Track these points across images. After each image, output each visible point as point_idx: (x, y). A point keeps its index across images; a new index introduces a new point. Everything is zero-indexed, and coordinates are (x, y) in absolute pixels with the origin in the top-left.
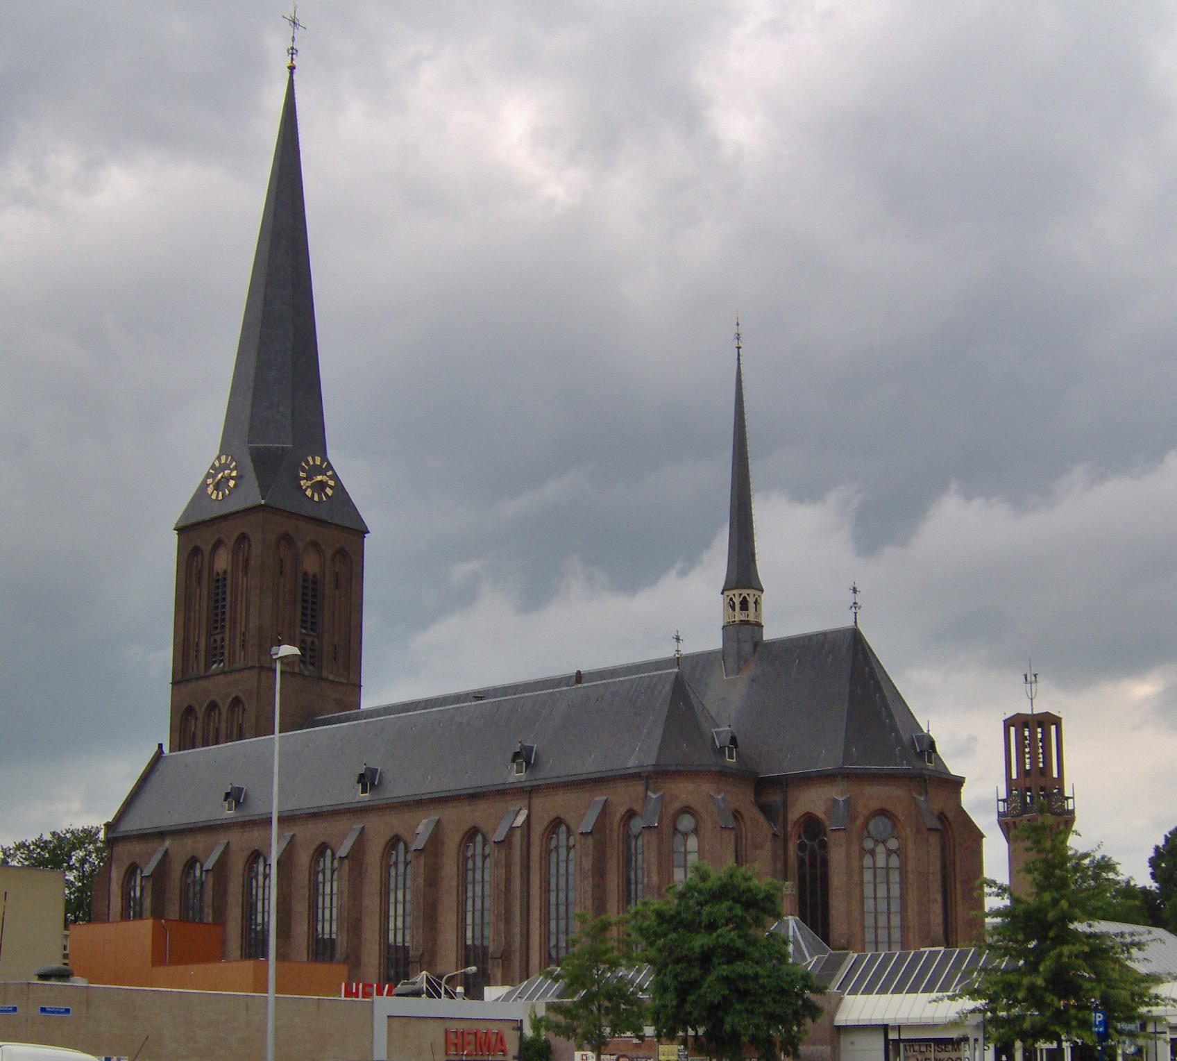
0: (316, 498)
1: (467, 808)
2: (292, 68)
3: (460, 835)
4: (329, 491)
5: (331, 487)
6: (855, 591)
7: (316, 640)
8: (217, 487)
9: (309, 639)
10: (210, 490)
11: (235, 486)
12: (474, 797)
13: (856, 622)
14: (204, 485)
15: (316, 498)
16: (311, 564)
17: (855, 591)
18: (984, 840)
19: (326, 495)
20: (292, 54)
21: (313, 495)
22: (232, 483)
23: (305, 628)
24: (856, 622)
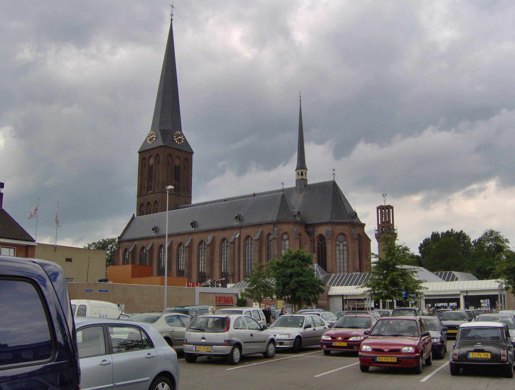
0: (179, 143)
1: (222, 233)
2: (172, 20)
3: (220, 240)
4: (182, 141)
5: (183, 140)
6: (334, 170)
7: (178, 184)
8: (150, 140)
9: (177, 184)
10: (148, 141)
11: (155, 140)
12: (224, 229)
13: (334, 179)
14: (146, 140)
15: (179, 143)
16: (177, 162)
17: (334, 170)
18: (371, 242)
19: (182, 142)
20: (172, 16)
21: (178, 142)
22: (154, 139)
23: (175, 181)
24: (334, 179)
